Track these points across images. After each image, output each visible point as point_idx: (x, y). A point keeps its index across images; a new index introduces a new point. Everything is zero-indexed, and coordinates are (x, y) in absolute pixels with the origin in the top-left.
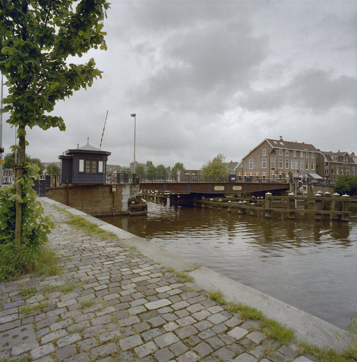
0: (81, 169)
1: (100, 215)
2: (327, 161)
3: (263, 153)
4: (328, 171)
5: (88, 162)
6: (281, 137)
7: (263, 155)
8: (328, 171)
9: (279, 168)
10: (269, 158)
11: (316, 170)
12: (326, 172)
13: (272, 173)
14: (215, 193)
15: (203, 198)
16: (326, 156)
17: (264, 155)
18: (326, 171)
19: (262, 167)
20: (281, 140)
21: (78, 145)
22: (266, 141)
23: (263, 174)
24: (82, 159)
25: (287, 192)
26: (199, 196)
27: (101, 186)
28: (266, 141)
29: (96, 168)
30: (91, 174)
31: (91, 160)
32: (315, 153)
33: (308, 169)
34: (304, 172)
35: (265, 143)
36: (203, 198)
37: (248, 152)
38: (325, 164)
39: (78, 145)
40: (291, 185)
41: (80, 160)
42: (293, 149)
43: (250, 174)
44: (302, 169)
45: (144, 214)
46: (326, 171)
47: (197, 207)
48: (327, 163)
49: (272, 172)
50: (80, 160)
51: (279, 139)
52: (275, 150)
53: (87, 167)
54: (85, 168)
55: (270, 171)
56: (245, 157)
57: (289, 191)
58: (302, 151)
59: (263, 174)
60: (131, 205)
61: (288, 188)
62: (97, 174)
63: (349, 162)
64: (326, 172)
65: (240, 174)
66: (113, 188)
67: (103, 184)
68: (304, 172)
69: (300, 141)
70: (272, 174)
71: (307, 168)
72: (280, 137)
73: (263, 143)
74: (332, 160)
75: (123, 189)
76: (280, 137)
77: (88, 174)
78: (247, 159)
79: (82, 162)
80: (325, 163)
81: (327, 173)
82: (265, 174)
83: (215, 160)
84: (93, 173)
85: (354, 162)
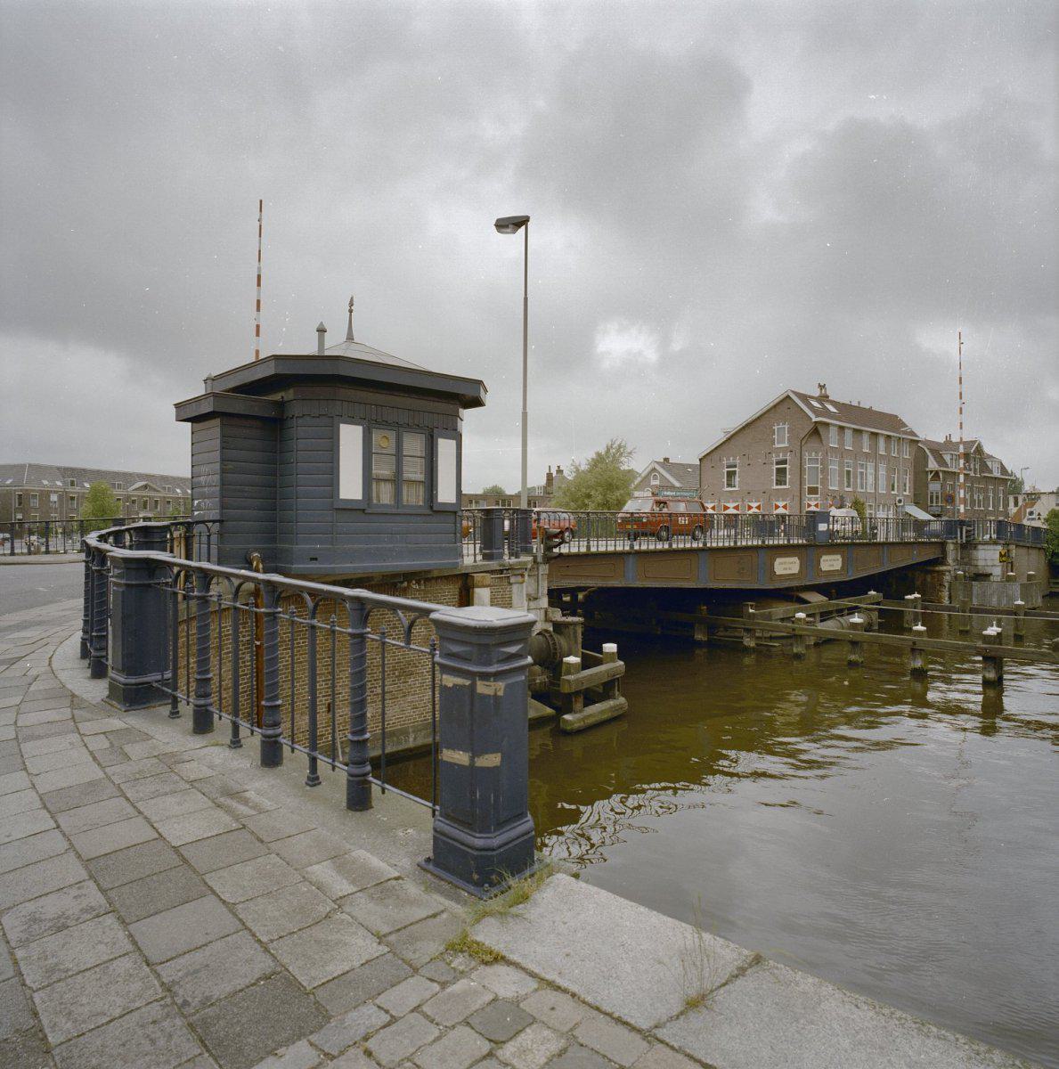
0: (350, 487)
1: (420, 742)
2: (937, 466)
3: (776, 437)
4: (937, 497)
5: (383, 440)
6: (822, 387)
7: (777, 446)
8: (937, 497)
9: (831, 488)
10: (798, 455)
11: (915, 495)
12: (932, 502)
13: (809, 506)
14: (777, 585)
15: (751, 611)
16: (931, 450)
17: (778, 443)
18: (932, 497)
19: (723, 485)
20: (824, 398)
21: (321, 331)
22: (788, 397)
23: (777, 507)
24: (352, 420)
25: (938, 572)
26: (733, 599)
27: (418, 582)
28: (788, 397)
29: (421, 477)
30: (398, 512)
31: (399, 428)
32: (912, 440)
33: (895, 492)
34: (900, 501)
35: (785, 405)
36: (751, 611)
37: (720, 437)
38: (930, 477)
39: (321, 331)
40: (950, 547)
41: (341, 425)
42: (882, 429)
43: (726, 508)
44: (862, 488)
45: (616, 714)
46: (932, 497)
47: (711, 645)
48: (937, 474)
49: (810, 499)
50: (341, 425)
51: (816, 393)
52: (821, 429)
53: (414, 471)
54: (368, 479)
55: (803, 498)
56: (712, 451)
57: (945, 568)
58: (882, 434)
59: (777, 507)
60: (571, 677)
61: (943, 558)
62: (429, 512)
63: (981, 471)
64: (932, 502)
65: (781, 504)
66: (477, 590)
67: (429, 571)
68: (900, 501)
69: (879, 407)
70: (727, 512)
71: (893, 490)
72: (820, 386)
73: (775, 406)
74: (947, 466)
75: (515, 588)
76: (820, 386)
77: (384, 514)
78: (716, 456)
79: (350, 438)
80: (931, 472)
81: (934, 504)
82: (785, 507)
83: (599, 460)
84: (378, 506)
85: (991, 472)
